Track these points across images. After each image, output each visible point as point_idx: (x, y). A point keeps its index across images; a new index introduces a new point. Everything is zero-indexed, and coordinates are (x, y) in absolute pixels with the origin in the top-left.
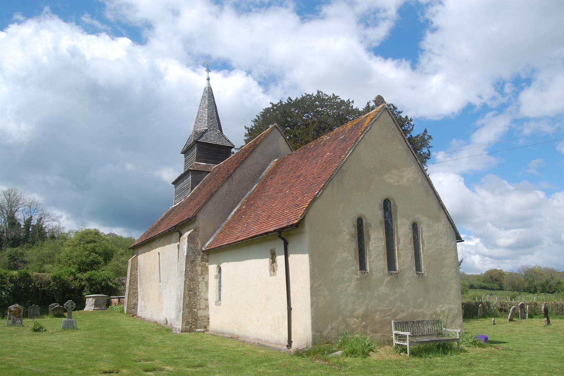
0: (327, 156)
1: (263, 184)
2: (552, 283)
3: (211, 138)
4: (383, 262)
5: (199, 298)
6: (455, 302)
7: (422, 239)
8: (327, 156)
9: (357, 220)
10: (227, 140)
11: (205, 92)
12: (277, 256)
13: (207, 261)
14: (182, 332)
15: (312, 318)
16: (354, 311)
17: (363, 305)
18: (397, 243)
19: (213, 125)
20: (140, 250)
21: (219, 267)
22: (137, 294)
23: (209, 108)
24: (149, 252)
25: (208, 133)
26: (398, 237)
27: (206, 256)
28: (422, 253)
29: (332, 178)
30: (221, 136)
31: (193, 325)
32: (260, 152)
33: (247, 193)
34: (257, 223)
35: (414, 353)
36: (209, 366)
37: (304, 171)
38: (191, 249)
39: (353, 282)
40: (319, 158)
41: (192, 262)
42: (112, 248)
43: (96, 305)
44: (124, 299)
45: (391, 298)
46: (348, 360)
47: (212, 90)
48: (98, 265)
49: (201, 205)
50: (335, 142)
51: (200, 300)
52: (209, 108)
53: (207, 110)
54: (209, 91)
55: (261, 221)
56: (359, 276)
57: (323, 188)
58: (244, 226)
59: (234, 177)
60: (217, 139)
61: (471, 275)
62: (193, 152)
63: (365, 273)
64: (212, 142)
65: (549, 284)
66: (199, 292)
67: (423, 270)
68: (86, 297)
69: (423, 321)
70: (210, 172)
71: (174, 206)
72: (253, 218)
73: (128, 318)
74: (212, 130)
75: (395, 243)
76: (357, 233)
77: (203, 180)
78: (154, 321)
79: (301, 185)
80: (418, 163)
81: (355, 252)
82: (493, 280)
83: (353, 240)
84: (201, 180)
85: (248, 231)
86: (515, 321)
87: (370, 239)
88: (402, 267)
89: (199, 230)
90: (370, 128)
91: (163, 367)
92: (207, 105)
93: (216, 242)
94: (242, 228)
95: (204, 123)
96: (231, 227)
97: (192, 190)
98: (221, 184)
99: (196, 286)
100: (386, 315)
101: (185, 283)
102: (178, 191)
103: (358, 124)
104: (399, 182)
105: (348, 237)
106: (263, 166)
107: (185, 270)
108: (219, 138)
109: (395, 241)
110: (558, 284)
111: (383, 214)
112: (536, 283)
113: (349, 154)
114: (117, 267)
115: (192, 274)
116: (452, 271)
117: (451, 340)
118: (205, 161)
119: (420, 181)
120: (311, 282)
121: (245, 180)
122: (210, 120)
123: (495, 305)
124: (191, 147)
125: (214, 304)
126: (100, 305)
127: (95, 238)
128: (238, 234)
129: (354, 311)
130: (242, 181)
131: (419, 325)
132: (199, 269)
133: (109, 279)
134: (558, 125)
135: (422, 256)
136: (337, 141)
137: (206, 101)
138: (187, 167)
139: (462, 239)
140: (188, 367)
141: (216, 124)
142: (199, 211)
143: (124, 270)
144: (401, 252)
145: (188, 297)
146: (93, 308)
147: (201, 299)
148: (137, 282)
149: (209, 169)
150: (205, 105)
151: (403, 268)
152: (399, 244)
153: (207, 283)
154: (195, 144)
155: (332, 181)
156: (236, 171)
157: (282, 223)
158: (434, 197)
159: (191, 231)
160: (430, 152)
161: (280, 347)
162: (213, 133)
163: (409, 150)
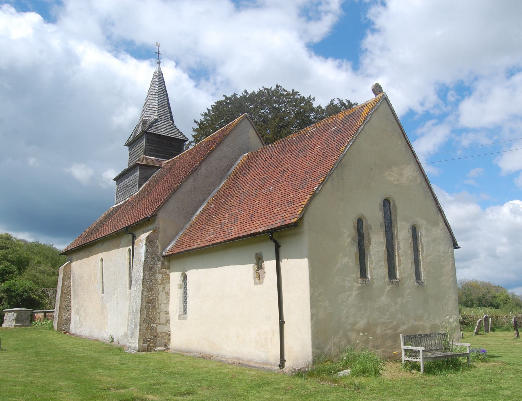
0: (318, 149)
1: (234, 180)
2: (488, 296)
3: (162, 130)
4: (384, 268)
5: (158, 311)
7: (422, 244)
8: (318, 149)
9: (357, 220)
10: (180, 133)
12: (264, 262)
13: (168, 268)
14: (139, 351)
16: (355, 324)
17: (365, 317)
18: (398, 248)
19: (163, 114)
20: (74, 257)
21: (184, 275)
22: (70, 307)
23: (160, 96)
24: (88, 258)
25: (159, 123)
26: (398, 242)
28: (421, 260)
29: (332, 171)
30: (174, 127)
31: (151, 343)
32: (229, 144)
33: (214, 190)
34: (235, 223)
35: (429, 370)
37: (290, 165)
38: (149, 254)
39: (354, 291)
40: (308, 151)
41: (151, 269)
42: (28, 255)
43: (18, 320)
46: (362, 379)
47: (163, 75)
48: (11, 275)
49: (162, 203)
50: (325, 133)
51: (159, 313)
52: (160, 96)
53: (157, 97)
54: (159, 75)
55: (241, 221)
58: (217, 227)
59: (200, 171)
60: (168, 131)
62: (140, 144)
63: (366, 281)
64: (163, 134)
65: (486, 298)
66: (158, 304)
67: (423, 279)
68: (4, 311)
69: (430, 334)
70: (161, 167)
71: (116, 205)
72: (228, 218)
73: (60, 336)
75: (395, 247)
78: (94, 339)
81: (356, 257)
83: (353, 244)
84: (150, 177)
86: (481, 334)
87: (371, 243)
88: (402, 275)
89: (159, 232)
90: (370, 118)
92: (158, 92)
94: (215, 229)
95: (153, 112)
97: (139, 187)
98: (185, 179)
99: (156, 297)
100: (387, 328)
101: (142, 293)
102: (121, 188)
104: (398, 180)
105: (349, 240)
106: (232, 160)
107: (142, 278)
108: (171, 130)
109: (395, 246)
110: (494, 298)
112: (473, 297)
114: (34, 277)
115: (151, 283)
116: (450, 280)
117: (462, 355)
118: (154, 155)
120: (310, 291)
121: (212, 175)
122: (161, 109)
124: (138, 139)
125: (178, 318)
127: (6, 244)
129: (355, 324)
130: (208, 176)
131: (427, 339)
132: (159, 277)
133: (31, 290)
134: (495, 138)
135: (421, 263)
136: (328, 132)
137: (156, 87)
138: (132, 161)
139: (459, 246)
141: (168, 114)
142: (159, 209)
143: (43, 280)
144: (401, 258)
145: (146, 310)
146: (14, 324)
147: (161, 312)
148: (70, 293)
149: (159, 164)
151: (404, 275)
152: (400, 249)
153: (168, 294)
154: (143, 135)
155: (331, 175)
156: (202, 165)
157: (274, 223)
159: (150, 232)
161: (270, 367)
162: (164, 124)
163: (408, 146)
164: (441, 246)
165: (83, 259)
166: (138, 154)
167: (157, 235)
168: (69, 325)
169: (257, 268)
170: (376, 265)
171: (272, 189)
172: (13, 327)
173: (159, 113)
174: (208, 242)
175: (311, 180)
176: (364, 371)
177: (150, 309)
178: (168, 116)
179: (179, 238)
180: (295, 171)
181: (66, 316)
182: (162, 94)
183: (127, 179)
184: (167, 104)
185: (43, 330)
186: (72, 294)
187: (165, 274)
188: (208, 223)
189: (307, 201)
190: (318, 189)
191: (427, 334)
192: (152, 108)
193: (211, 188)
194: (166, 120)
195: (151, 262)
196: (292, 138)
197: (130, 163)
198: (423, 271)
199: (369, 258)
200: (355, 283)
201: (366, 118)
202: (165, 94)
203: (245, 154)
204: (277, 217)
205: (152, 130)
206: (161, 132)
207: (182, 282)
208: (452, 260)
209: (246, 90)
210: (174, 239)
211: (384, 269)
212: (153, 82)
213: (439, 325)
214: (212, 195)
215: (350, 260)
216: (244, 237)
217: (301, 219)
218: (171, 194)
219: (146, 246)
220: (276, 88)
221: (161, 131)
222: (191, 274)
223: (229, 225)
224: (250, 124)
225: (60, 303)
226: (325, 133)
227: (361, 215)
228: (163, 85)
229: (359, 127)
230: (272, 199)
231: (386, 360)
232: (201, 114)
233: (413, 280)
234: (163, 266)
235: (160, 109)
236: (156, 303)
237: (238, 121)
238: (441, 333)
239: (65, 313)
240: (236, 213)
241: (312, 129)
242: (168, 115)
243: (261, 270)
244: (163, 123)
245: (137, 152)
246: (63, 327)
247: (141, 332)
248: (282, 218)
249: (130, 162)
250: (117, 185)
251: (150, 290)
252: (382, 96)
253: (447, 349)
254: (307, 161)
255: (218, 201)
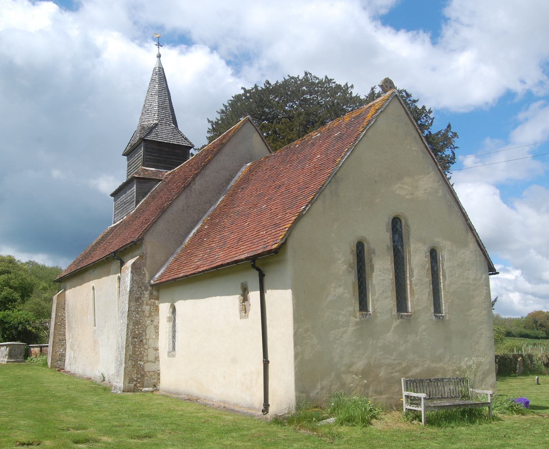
1: (232, 195)
4: (390, 300)
5: (146, 347)
6: (486, 355)
7: (443, 270)
11: (155, 73)
12: (249, 292)
13: (157, 298)
14: (123, 391)
15: (296, 374)
16: (351, 365)
17: (364, 357)
18: (410, 276)
20: (68, 284)
21: (173, 306)
22: (64, 341)
23: (160, 95)
26: (410, 268)
27: (156, 292)
28: (442, 289)
29: (323, 188)
30: (176, 132)
31: (138, 383)
33: (210, 207)
35: (430, 422)
36: (160, 436)
37: (287, 178)
38: (135, 283)
39: (350, 327)
40: (307, 162)
41: (137, 299)
44: (47, 348)
45: (401, 349)
46: (344, 429)
48: (13, 303)
49: (149, 225)
50: (327, 140)
51: (147, 349)
52: (160, 95)
53: (157, 97)
54: (160, 72)
55: (228, 246)
56: (358, 319)
57: (312, 202)
58: (206, 252)
60: (170, 136)
61: (508, 318)
62: (138, 154)
63: (366, 315)
64: (164, 140)
66: (146, 339)
67: (444, 312)
70: (161, 180)
73: (53, 373)
74: (164, 124)
76: (356, 261)
77: (152, 191)
78: (87, 377)
79: (282, 197)
80: (439, 170)
81: (354, 287)
82: (538, 325)
83: (350, 272)
84: (149, 191)
85: (211, 259)
88: (415, 308)
89: (146, 257)
91: (99, 438)
92: (158, 91)
93: (169, 273)
95: (153, 115)
96: (189, 252)
97: (137, 204)
98: (176, 196)
100: (394, 371)
101: (128, 327)
102: (119, 205)
103: (358, 117)
107: (127, 310)
108: (174, 135)
109: (407, 273)
111: (392, 237)
113: (347, 156)
115: (137, 316)
117: (480, 405)
118: (154, 165)
119: (441, 193)
120: (294, 326)
121: (208, 191)
122: (162, 111)
123: (540, 359)
126: (15, 355)
127: (9, 267)
128: (198, 263)
129: (351, 365)
130: (203, 192)
132: (146, 308)
135: (442, 293)
137: (156, 85)
138: (131, 174)
139: (497, 271)
140: (132, 438)
141: (170, 116)
142: (146, 232)
144: (415, 288)
146: (6, 360)
147: (149, 348)
148: (65, 325)
149: (160, 177)
150: (155, 91)
151: (417, 308)
152: (413, 277)
153: (157, 328)
154: (141, 143)
158: (459, 214)
159: (136, 258)
160: (454, 154)
162: (165, 128)
164: (470, 272)
165: (76, 287)
166: (136, 165)
167: (144, 261)
168: (63, 362)
169: (243, 300)
170: (381, 296)
171: (264, 208)
172: (5, 363)
173: (160, 116)
174: (194, 270)
175: (301, 198)
176: (349, 419)
177: (136, 345)
178: (170, 119)
179: (169, 264)
180: (290, 186)
181: (60, 352)
182: (162, 94)
183: (124, 195)
184: (169, 105)
185: (36, 367)
186: (66, 327)
187: (153, 305)
188: (198, 247)
189: (292, 223)
190: (306, 210)
191: (439, 379)
192: (151, 111)
193: (207, 206)
194: (168, 124)
195: (137, 292)
196: (296, 145)
197: (129, 175)
198: (444, 303)
199: (371, 288)
200: (351, 317)
201: (369, 122)
202: (167, 93)
203: (247, 164)
204: (261, 241)
205: (151, 137)
206: (162, 139)
207: (171, 315)
208: (486, 289)
209: (268, 80)
210: (164, 266)
211: (392, 301)
212: (152, 80)
213: (455, 369)
214: (208, 213)
215: (346, 291)
216: (228, 264)
217: (283, 246)
218: (160, 214)
219: (132, 274)
220: (305, 76)
221: (162, 137)
222: (180, 305)
223: (217, 250)
224: (254, 128)
225: (54, 337)
226: (327, 140)
227: (362, 237)
228: (165, 83)
229: (360, 133)
230: (261, 220)
231: (391, 408)
232: (217, 111)
233: (430, 314)
234: (151, 296)
235: (160, 111)
236: (143, 338)
237: (239, 125)
238: (458, 378)
239: (59, 348)
240: (226, 236)
241: (316, 135)
242: (170, 118)
243: (247, 302)
244: (164, 128)
245: (135, 162)
246: (58, 364)
247: (126, 371)
248: (265, 243)
249: (128, 174)
250: (115, 201)
251: (137, 323)
252: (392, 94)
253: (465, 396)
254: (303, 175)
255: (212, 221)
